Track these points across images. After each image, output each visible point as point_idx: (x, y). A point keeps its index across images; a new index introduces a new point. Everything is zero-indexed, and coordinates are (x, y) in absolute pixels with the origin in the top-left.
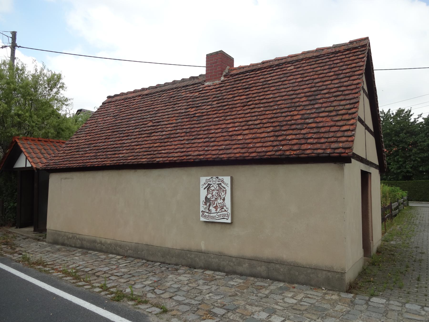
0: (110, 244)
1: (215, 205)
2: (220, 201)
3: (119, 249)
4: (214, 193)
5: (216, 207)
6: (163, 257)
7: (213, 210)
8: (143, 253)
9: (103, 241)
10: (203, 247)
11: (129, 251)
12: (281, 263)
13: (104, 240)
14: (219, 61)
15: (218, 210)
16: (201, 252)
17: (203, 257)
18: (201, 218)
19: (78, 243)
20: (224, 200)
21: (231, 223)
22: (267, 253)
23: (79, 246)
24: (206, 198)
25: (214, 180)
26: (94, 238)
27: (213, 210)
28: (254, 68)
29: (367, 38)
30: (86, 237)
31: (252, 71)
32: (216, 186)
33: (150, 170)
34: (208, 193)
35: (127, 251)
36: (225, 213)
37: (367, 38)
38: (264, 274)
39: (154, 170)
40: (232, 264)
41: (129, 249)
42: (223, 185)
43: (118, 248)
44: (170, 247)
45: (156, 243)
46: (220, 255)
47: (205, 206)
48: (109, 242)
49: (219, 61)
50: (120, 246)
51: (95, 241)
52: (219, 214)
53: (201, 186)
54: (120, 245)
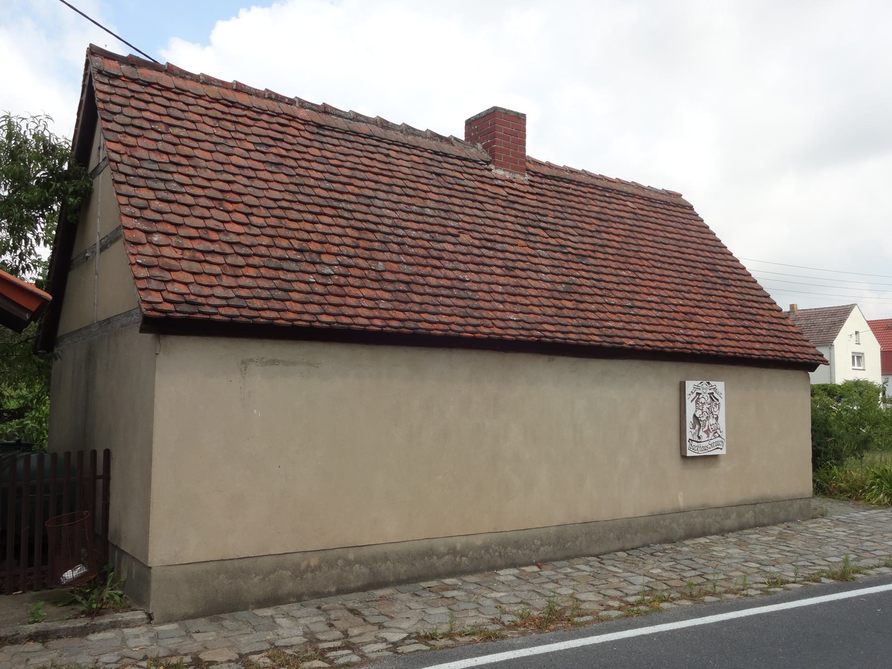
0: (486, 547)
1: (706, 428)
2: (712, 421)
3: (514, 551)
4: (705, 407)
5: (707, 432)
6: (619, 539)
7: (704, 436)
8: (578, 543)
9: (459, 543)
10: (681, 503)
11: (542, 549)
12: (765, 501)
13: (464, 539)
14: (498, 130)
15: (711, 435)
16: (679, 511)
17: (681, 520)
18: (688, 451)
19: (358, 574)
20: (717, 419)
21: (684, 457)
22: (754, 491)
23: (360, 584)
24: (695, 415)
25: (705, 386)
26: (426, 542)
27: (704, 436)
28: (636, 192)
29: (91, 45)
30: (390, 548)
31: (553, 178)
32: (707, 396)
33: (584, 359)
34: (697, 408)
35: (538, 549)
36: (719, 439)
37: (91, 45)
38: (752, 522)
39: (595, 360)
40: (719, 519)
41: (542, 545)
42: (715, 395)
43: (512, 551)
44: (630, 515)
45: (605, 514)
46: (704, 509)
47: (693, 431)
48: (478, 541)
49: (498, 130)
50: (518, 545)
51: (429, 553)
52: (712, 441)
53: (687, 397)
54: (516, 542)
